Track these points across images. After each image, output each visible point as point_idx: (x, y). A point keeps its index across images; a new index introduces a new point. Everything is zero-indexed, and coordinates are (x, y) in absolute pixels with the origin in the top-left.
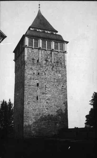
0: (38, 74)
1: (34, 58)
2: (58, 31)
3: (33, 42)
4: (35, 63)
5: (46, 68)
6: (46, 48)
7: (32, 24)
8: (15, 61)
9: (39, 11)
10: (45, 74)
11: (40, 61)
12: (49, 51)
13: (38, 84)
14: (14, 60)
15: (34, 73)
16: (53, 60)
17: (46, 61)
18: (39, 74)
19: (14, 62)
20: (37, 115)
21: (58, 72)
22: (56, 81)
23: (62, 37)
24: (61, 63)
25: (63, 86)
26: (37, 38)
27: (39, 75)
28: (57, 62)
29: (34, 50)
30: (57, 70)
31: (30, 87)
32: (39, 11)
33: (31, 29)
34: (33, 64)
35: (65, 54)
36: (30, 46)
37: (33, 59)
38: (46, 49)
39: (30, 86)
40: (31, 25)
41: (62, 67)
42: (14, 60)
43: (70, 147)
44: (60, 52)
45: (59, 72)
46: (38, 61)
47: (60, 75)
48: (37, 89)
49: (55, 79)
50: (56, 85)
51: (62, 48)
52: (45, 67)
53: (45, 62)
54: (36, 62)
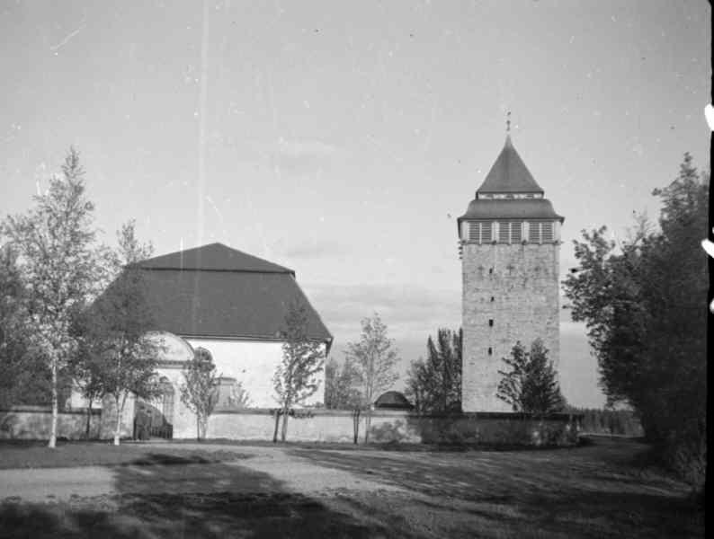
0: (493, 299)
1: (484, 266)
3: (481, 230)
4: (485, 275)
7: (485, 184)
9: (508, 139)
11: (495, 271)
12: (518, 245)
13: (491, 323)
16: (528, 264)
17: (511, 268)
22: (532, 312)
24: (546, 270)
25: (549, 323)
26: (488, 220)
28: (536, 269)
31: (475, 329)
32: (508, 139)
33: (482, 197)
34: (481, 278)
35: (557, 247)
37: (481, 268)
38: (541, 242)
40: (482, 180)
41: (547, 279)
45: (542, 291)
46: (491, 271)
48: (490, 332)
49: (530, 308)
51: (548, 234)
52: (508, 283)
53: (508, 271)
54: (486, 273)
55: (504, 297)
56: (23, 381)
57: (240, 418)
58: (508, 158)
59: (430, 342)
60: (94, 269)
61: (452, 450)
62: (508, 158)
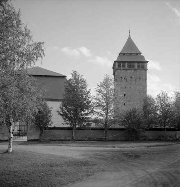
0: (125, 88)
17: (131, 78)
37: (121, 78)
52: (130, 82)
53: (130, 79)
55: (129, 87)
56: (44, 103)
57: (54, 131)
58: (130, 43)
59: (58, 112)
60: (29, 65)
61: (144, 141)
62: (130, 43)
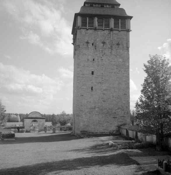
2: (120, 3)
5: (104, 52)
6: (104, 28)
8: (74, 45)
10: (102, 60)
14: (72, 44)
15: (88, 60)
18: (95, 60)
19: (73, 46)
20: (92, 108)
21: (118, 56)
23: (125, 11)
27: (95, 61)
29: (88, 31)
30: (117, 54)
35: (88, 44)
36: (101, 28)
38: (120, 29)
39: (83, 74)
42: (72, 44)
43: (137, 68)
44: (121, 30)
47: (121, 60)
50: (115, 73)
53: (102, 45)
